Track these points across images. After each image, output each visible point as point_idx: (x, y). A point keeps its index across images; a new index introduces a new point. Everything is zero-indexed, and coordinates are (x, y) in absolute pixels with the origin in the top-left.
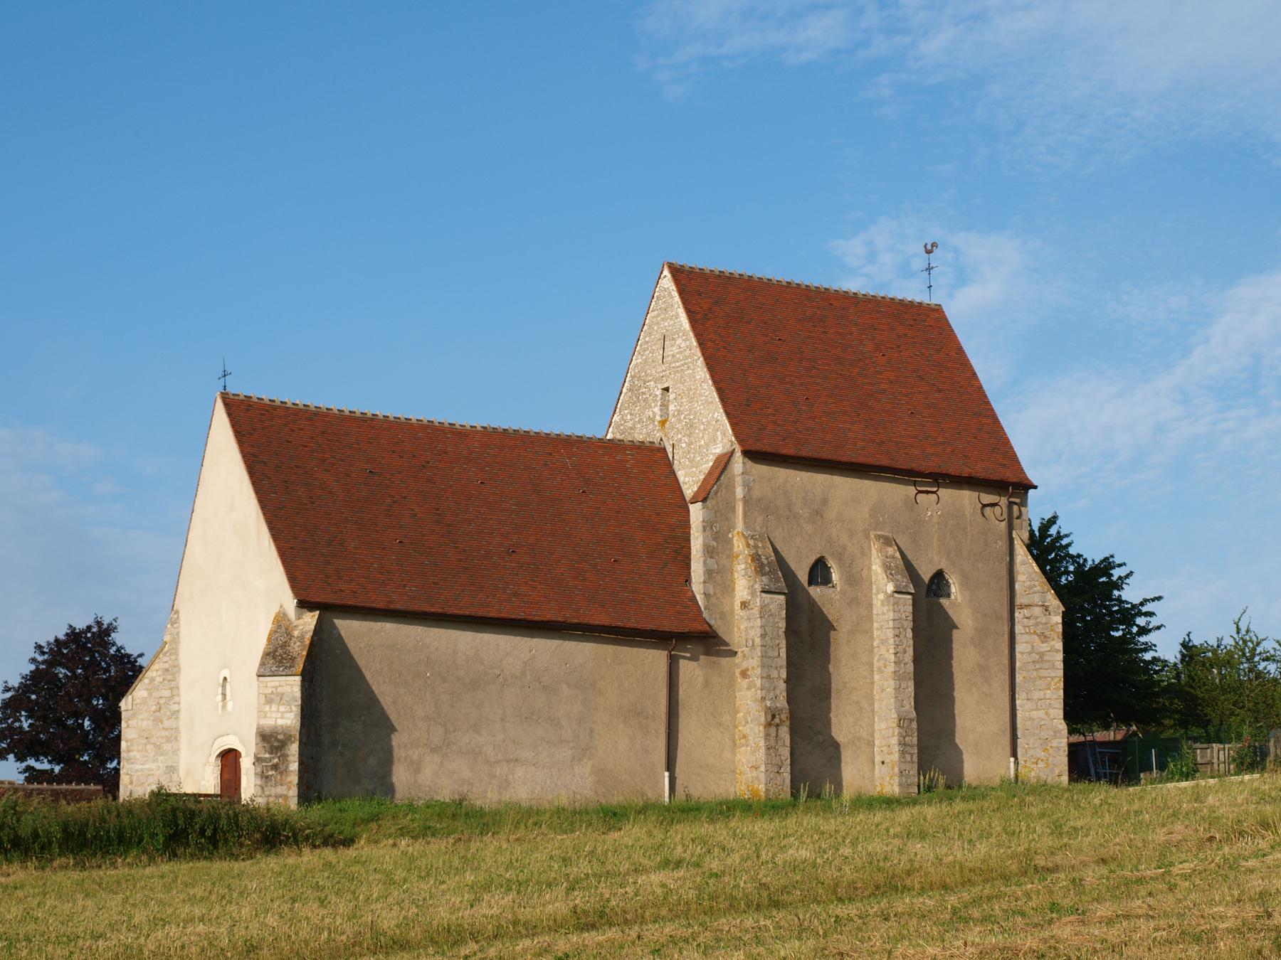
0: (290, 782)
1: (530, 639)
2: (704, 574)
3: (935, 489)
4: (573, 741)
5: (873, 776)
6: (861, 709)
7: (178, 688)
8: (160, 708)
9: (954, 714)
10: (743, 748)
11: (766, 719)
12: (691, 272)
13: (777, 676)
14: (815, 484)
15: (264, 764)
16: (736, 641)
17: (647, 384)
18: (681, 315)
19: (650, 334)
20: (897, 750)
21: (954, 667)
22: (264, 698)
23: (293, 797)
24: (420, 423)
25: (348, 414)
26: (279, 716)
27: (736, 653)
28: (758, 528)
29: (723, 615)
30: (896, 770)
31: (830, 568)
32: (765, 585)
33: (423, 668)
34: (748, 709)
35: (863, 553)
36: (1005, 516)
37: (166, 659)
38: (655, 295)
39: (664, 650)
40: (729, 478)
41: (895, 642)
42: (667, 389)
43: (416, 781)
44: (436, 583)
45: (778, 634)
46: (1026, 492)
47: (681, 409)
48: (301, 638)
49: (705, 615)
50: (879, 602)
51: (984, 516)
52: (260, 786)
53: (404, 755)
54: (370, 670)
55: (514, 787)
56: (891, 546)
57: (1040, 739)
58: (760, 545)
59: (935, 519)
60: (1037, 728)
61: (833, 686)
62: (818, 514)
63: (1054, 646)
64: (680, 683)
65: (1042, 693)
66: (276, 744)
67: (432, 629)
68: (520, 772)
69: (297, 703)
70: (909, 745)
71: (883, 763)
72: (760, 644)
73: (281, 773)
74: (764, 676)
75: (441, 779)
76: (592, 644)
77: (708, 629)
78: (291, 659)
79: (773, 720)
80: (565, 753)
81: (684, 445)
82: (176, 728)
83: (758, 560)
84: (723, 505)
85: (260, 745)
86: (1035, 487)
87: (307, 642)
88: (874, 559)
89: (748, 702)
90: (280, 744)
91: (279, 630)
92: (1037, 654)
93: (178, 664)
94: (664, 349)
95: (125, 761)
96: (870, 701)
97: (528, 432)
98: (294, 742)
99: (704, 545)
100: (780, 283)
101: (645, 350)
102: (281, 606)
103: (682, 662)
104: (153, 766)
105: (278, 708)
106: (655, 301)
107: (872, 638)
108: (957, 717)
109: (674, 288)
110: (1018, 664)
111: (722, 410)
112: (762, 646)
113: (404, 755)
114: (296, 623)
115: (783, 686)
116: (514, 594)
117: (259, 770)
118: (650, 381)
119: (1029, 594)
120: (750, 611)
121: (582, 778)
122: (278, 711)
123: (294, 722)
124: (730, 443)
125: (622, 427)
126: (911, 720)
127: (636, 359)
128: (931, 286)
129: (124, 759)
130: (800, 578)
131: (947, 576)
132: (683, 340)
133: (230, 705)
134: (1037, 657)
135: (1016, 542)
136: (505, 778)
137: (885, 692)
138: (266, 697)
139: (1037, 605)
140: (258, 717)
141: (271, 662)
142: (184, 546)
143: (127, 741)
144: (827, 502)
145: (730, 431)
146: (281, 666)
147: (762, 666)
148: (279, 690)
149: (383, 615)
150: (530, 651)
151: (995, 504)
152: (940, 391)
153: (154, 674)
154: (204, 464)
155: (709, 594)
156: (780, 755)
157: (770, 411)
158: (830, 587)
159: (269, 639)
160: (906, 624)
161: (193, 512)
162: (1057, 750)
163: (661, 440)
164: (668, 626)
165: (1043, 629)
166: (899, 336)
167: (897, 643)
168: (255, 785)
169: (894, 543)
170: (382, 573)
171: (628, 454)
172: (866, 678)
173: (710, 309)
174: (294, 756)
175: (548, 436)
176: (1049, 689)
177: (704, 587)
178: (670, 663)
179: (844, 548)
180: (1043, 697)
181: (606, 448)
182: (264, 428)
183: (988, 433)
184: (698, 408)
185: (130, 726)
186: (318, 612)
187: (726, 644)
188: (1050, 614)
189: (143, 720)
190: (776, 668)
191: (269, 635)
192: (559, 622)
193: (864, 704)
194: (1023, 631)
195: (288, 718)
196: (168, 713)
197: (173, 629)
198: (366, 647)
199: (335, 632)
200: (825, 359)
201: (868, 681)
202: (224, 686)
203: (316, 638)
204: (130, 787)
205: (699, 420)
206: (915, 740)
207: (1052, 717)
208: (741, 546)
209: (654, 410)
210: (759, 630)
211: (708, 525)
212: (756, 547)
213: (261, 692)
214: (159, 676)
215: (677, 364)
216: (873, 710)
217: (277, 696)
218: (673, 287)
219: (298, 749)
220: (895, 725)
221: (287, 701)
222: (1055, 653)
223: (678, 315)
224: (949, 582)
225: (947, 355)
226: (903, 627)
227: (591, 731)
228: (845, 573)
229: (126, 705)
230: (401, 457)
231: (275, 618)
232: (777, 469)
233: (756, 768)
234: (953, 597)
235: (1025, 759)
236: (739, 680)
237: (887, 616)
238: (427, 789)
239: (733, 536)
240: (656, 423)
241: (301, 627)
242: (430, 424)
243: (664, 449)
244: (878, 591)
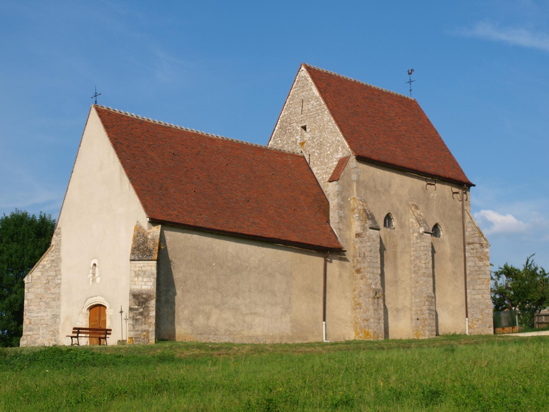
0: (150, 323)
7: (60, 271)
8: (49, 282)
10: (358, 310)
17: (291, 125)
18: (313, 89)
19: (293, 100)
26: (143, 284)
31: (391, 219)
34: (361, 289)
37: (52, 255)
38: (296, 80)
46: (469, 188)
47: (314, 136)
52: (132, 324)
53: (202, 309)
55: (254, 329)
57: (479, 309)
65: (480, 286)
69: (154, 277)
73: (145, 317)
80: (278, 310)
81: (316, 154)
86: (474, 186)
89: (361, 286)
90: (144, 300)
92: (478, 267)
94: (302, 106)
95: (26, 311)
98: (152, 299)
101: (290, 108)
102: (138, 222)
105: (143, 279)
106: (296, 83)
111: (341, 136)
113: (202, 309)
114: (148, 231)
117: (131, 315)
118: (294, 123)
120: (362, 238)
123: (152, 287)
127: (284, 113)
128: (411, 90)
129: (26, 310)
132: (315, 102)
133: (98, 280)
134: (478, 268)
136: (250, 323)
137: (418, 283)
139: (477, 243)
142: (66, 191)
143: (28, 300)
145: (348, 146)
146: (145, 255)
148: (143, 268)
151: (457, 193)
153: (45, 263)
154: (81, 145)
155: (341, 229)
157: (362, 138)
161: (72, 173)
171: (288, 158)
176: (484, 284)
180: (480, 288)
184: (326, 135)
189: (38, 288)
194: (470, 256)
195: (148, 285)
202: (94, 270)
204: (29, 326)
205: (326, 141)
207: (485, 298)
212: (363, 205)
214: (49, 264)
215: (311, 114)
218: (308, 76)
219: (155, 304)
221: (148, 275)
223: (312, 89)
224: (439, 230)
227: (290, 299)
229: (27, 280)
231: (135, 228)
234: (441, 237)
235: (472, 319)
237: (419, 245)
240: (298, 144)
241: (152, 234)
243: (304, 157)
244: (414, 232)
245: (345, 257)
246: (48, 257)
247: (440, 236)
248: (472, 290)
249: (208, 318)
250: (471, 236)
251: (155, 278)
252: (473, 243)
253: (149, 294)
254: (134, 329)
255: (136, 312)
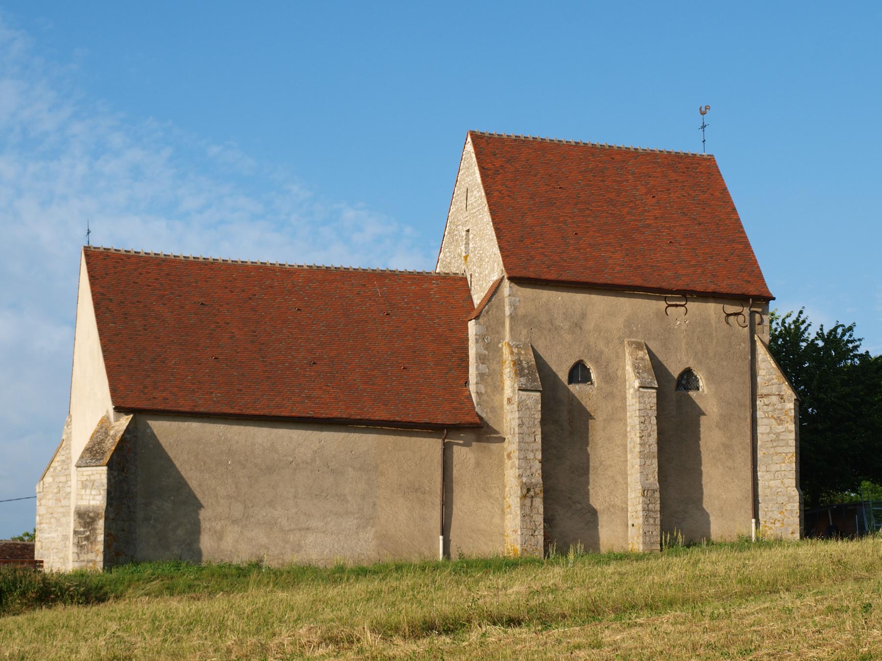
0: (98, 550)
1: (319, 432)
2: (477, 377)
3: (684, 303)
4: (358, 513)
5: (627, 536)
6: (616, 482)
7: (70, 475)
8: (59, 491)
9: (701, 485)
11: (522, 492)
12: (490, 138)
13: (532, 457)
14: (574, 302)
15: (79, 536)
16: (505, 430)
20: (642, 515)
21: (701, 447)
22: (81, 484)
23: (100, 561)
24: (254, 264)
25: (192, 259)
26: (91, 498)
27: (505, 439)
28: (523, 339)
29: (493, 410)
30: (641, 531)
31: (589, 369)
32: (522, 385)
33: (224, 458)
35: (617, 357)
36: (747, 323)
37: (63, 453)
39: (439, 438)
40: (499, 300)
41: (640, 427)
42: (468, 231)
43: (219, 547)
44: (241, 390)
45: (534, 424)
46: (768, 303)
48: (115, 436)
49: (478, 409)
50: (630, 395)
51: (728, 323)
52: (77, 553)
53: (208, 526)
54: (179, 460)
55: (305, 550)
56: (642, 350)
57: (777, 503)
58: (523, 352)
59: (683, 327)
60: (775, 495)
61: (591, 464)
62: (577, 326)
63: (788, 427)
64: (454, 465)
66: (88, 520)
67: (233, 426)
68: (311, 538)
70: (652, 511)
71: (633, 525)
72: (517, 432)
73: (91, 543)
74: (522, 457)
75: (241, 544)
76: (374, 435)
77: (478, 421)
78: (102, 453)
79: (528, 493)
80: (350, 523)
82: (69, 506)
83: (519, 364)
84: (493, 321)
85: (77, 521)
86: (774, 299)
87: (118, 439)
88: (628, 361)
90: (91, 520)
91: (100, 430)
92: (774, 434)
93: (70, 457)
96: (624, 476)
97: (348, 269)
98: (101, 518)
99: (477, 354)
100: (569, 144)
103: (455, 448)
104: (54, 535)
105: (91, 492)
107: (625, 425)
108: (703, 487)
109: (473, 150)
110: (759, 443)
112: (519, 433)
113: (208, 526)
115: (538, 465)
116: (309, 397)
119: (768, 385)
121: (366, 542)
122: (91, 494)
123: (102, 502)
124: (501, 272)
125: (444, 263)
126: (654, 491)
128: (703, 142)
130: (561, 378)
131: (695, 373)
134: (775, 436)
135: (757, 344)
136: (298, 543)
138: (82, 483)
139: (774, 395)
140: (77, 499)
141: (88, 456)
143: (40, 516)
144: (586, 316)
146: (94, 459)
147: (519, 449)
148: (92, 477)
149: (190, 416)
150: (320, 442)
152: (700, 224)
155: (481, 393)
156: (534, 521)
158: (588, 384)
159: (91, 438)
160: (650, 413)
162: (790, 512)
163: (465, 271)
164: (441, 419)
165: (779, 414)
166: (670, 181)
167: (642, 428)
168: (73, 553)
169: (645, 347)
170: (194, 384)
171: (434, 284)
172: (620, 457)
173: (502, 166)
174: (101, 529)
175: (365, 271)
176: (784, 462)
177: (477, 387)
178: (444, 449)
179: (601, 353)
180: (779, 470)
181: (415, 279)
182: (116, 273)
183: (739, 256)
185: (42, 504)
186: (132, 416)
187: (496, 432)
188: (784, 402)
190: (532, 451)
191: (93, 434)
192: (344, 418)
193: (619, 478)
194: (763, 416)
195: (98, 500)
196: (64, 495)
197: (68, 430)
198: (175, 442)
199: (148, 431)
200: (599, 202)
201: (622, 459)
203: (128, 436)
204: (41, 551)
206: (658, 507)
208: (507, 355)
209: (461, 248)
210: (517, 420)
211: (480, 338)
213: (79, 479)
215: (474, 211)
216: (626, 483)
217: (90, 482)
219: (103, 524)
220: (640, 495)
221: (97, 486)
222: (788, 433)
224: (697, 378)
225: (712, 194)
226: (647, 415)
227: (374, 505)
228: (602, 373)
230: (232, 292)
232: (540, 291)
233: (516, 532)
234: (701, 390)
235: (765, 520)
236: (507, 461)
238: (229, 553)
239: (502, 346)
240: (462, 258)
242: (263, 265)
243: (466, 279)
245: (499, 435)
246: (59, 456)
247: (698, 389)
248: (765, 473)
249: (220, 538)
250: (765, 383)
251: (105, 490)
252: (767, 395)
253: (97, 511)
254: (79, 559)
255: (81, 536)
